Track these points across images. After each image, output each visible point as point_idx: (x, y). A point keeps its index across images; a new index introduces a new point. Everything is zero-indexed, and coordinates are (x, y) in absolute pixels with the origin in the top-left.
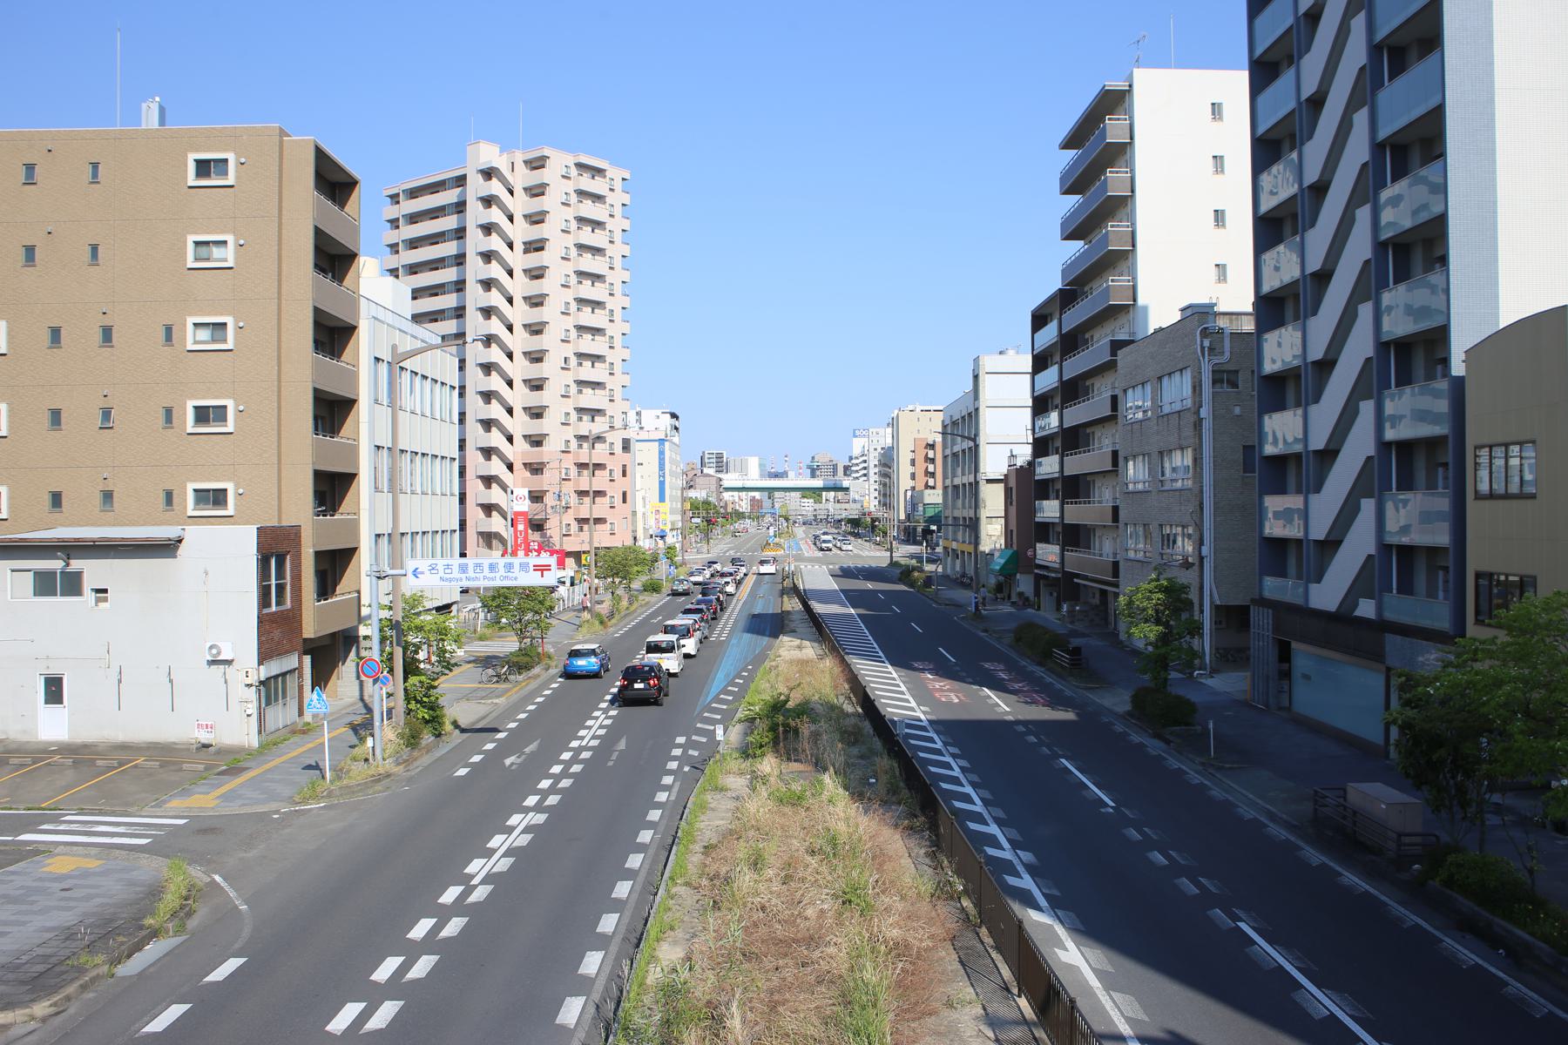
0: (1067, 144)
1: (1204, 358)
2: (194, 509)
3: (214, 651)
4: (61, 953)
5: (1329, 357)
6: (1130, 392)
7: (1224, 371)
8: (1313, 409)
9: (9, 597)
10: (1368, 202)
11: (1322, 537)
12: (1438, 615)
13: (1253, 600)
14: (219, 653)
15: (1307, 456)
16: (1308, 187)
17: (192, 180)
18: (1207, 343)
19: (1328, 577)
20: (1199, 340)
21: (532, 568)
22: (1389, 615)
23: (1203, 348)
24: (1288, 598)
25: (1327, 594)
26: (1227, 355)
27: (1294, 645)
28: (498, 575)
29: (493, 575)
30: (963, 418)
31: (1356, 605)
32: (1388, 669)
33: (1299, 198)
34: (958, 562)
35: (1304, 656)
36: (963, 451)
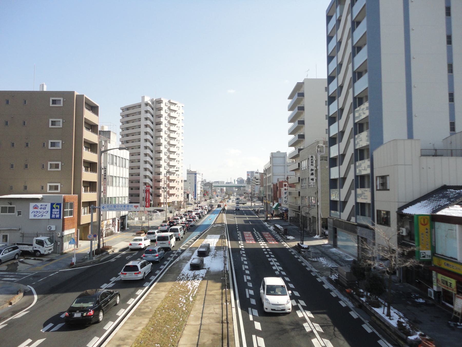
3: (50, 228)
7: (323, 157)
8: (341, 166)
10: (353, 138)
15: (340, 179)
18: (319, 149)
21: (134, 206)
22: (358, 222)
23: (318, 151)
27: (338, 229)
32: (358, 236)
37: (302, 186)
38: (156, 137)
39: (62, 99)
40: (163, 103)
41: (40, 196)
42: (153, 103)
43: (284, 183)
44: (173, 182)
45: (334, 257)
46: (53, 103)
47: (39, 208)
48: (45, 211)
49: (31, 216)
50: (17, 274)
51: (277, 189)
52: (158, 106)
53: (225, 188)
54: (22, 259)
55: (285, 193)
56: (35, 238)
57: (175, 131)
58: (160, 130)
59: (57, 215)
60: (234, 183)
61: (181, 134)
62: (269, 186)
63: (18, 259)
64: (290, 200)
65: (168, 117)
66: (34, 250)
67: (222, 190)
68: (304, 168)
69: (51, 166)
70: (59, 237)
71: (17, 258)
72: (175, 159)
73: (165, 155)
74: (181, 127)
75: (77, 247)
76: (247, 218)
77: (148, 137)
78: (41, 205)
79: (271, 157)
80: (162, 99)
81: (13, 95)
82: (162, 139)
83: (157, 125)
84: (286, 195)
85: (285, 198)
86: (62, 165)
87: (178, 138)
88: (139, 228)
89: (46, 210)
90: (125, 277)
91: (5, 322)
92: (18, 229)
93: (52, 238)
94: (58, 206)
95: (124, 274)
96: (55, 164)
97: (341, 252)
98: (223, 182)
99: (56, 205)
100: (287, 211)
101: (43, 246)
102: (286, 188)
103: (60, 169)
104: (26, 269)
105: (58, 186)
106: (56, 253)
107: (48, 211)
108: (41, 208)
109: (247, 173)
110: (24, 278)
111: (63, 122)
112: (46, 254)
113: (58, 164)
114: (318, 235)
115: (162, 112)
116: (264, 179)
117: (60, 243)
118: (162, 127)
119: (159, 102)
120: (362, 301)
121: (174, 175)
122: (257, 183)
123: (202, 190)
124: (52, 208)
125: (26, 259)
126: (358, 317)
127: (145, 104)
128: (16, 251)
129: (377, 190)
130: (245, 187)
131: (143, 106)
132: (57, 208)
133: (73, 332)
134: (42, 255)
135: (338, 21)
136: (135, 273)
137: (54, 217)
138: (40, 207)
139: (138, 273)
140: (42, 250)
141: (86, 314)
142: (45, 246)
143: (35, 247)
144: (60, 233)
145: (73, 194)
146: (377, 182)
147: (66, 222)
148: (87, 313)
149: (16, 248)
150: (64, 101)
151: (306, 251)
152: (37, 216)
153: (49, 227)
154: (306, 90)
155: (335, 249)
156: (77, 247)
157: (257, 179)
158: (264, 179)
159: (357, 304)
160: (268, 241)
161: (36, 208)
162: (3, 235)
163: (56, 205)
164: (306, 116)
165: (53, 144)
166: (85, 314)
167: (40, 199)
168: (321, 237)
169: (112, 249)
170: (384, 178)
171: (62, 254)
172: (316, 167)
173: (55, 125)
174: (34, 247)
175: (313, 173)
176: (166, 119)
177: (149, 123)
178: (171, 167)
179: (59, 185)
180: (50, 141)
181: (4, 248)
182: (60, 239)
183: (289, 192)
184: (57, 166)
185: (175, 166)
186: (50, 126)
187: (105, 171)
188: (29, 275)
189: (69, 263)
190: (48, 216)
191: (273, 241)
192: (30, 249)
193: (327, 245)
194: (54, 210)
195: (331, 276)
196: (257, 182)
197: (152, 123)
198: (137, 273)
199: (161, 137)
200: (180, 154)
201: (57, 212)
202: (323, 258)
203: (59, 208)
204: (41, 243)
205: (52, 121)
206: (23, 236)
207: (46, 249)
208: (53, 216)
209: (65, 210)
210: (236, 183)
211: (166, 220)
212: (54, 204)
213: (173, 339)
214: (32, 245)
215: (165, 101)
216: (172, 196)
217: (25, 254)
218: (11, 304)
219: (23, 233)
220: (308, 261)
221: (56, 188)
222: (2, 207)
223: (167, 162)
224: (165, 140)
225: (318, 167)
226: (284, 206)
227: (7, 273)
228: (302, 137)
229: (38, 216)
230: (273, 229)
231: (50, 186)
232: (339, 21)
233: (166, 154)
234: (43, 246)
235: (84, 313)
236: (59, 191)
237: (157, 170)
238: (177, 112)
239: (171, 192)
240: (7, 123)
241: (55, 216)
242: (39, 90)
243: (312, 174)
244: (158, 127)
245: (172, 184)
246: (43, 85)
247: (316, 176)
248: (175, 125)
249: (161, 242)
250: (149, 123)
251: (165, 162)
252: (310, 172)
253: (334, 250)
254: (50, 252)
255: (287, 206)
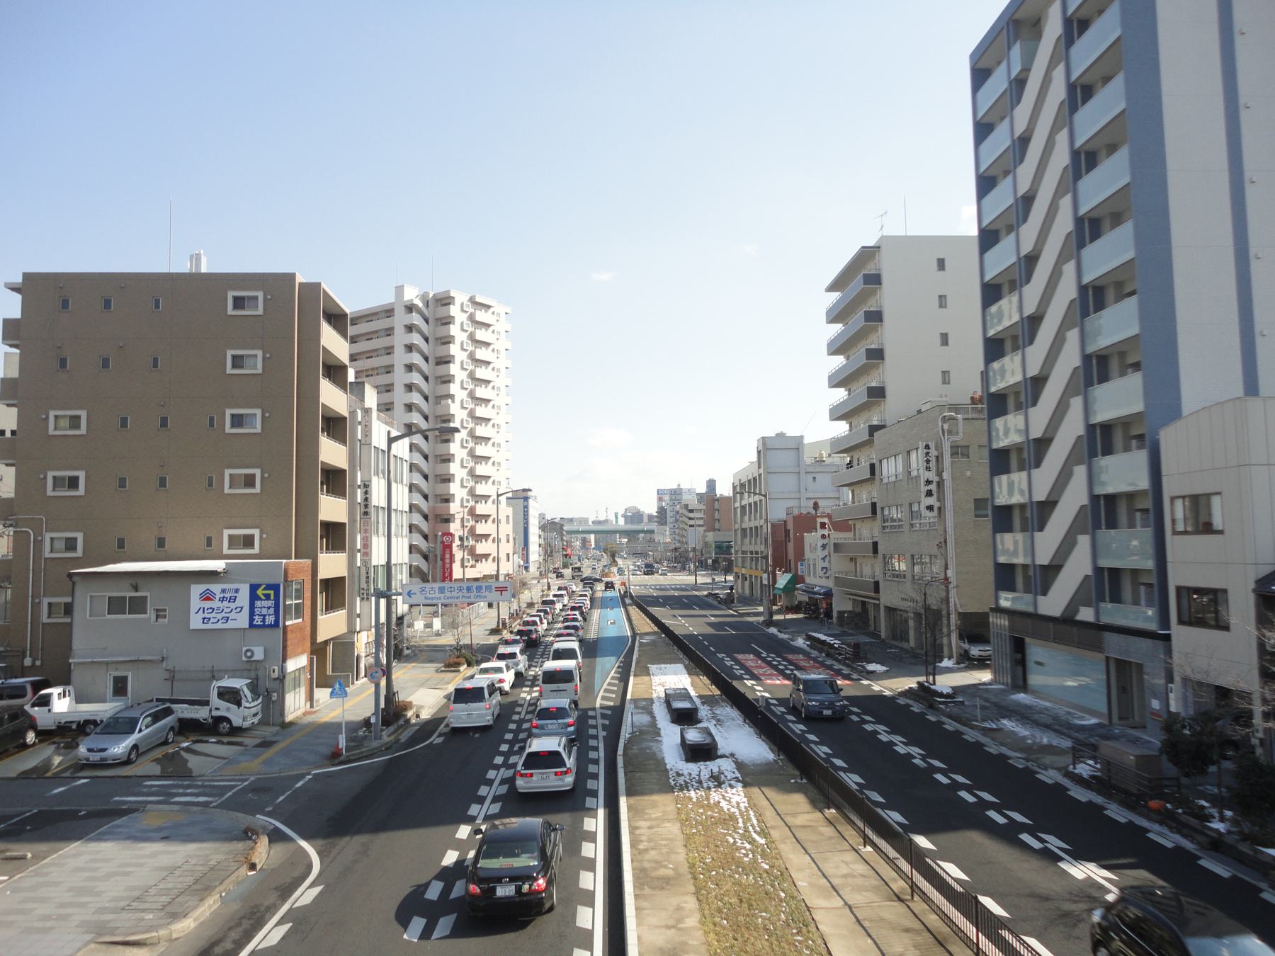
0: (832, 288)
1: (944, 435)
2: (229, 548)
3: (249, 654)
4: (179, 886)
5: (1051, 499)
6: (884, 462)
7: (958, 447)
9: (88, 616)
10: (1076, 326)
11: (1043, 499)
12: (1145, 617)
13: (992, 609)
14: (252, 655)
16: (1028, 316)
17: (230, 311)
18: (946, 427)
19: (1052, 592)
20: (940, 424)
21: (494, 589)
22: (1105, 619)
23: (943, 431)
24: (1021, 607)
25: (1053, 603)
26: (961, 434)
27: (1027, 640)
28: (472, 595)
29: (468, 595)
30: (749, 481)
31: (1077, 611)
32: (1107, 658)
33: (1027, 342)
34: (747, 583)
35: (1037, 651)
36: (750, 504)
37: (912, 525)
38: (437, 397)
39: (260, 295)
40: (454, 305)
41: (218, 565)
42: (427, 304)
43: (819, 520)
44: (484, 521)
45: (1036, 717)
46: (236, 307)
47: (218, 597)
48: (233, 605)
49: (196, 622)
50: (200, 783)
51: (786, 536)
52: (441, 312)
53: (592, 536)
54: (187, 744)
55: (824, 547)
56: (216, 684)
57: (489, 382)
58: (448, 380)
59: (267, 617)
60: (614, 522)
61: (503, 389)
62: (756, 528)
63: (173, 742)
64: (839, 565)
65: (469, 342)
66: (212, 717)
67: (584, 541)
68: (893, 479)
69: (57, 482)
70: (275, 679)
71: (170, 740)
72: (489, 458)
73: (462, 447)
74: (503, 370)
75: (312, 706)
76: (712, 616)
77: (416, 398)
78: (223, 591)
79: (761, 448)
80: (452, 294)
81: (61, 285)
82: (453, 402)
83: (438, 363)
84: (826, 552)
85: (823, 559)
86: (262, 478)
87: (496, 401)
88: (445, 651)
89: (238, 603)
90: (528, 785)
91: (282, 918)
92: (159, 658)
93: (255, 682)
94: (272, 592)
95: (526, 775)
96: (245, 475)
97: (1047, 704)
98: (586, 520)
99: (264, 589)
100: (828, 594)
101: (239, 704)
102: (826, 532)
103: (257, 489)
104: (215, 771)
105: (252, 536)
106: (267, 724)
107: (242, 608)
108: (222, 600)
109: (658, 494)
110: (230, 796)
111: (264, 358)
112: (248, 726)
113: (254, 476)
114: (949, 659)
115: (454, 330)
116: (735, 509)
117: (278, 696)
118: (454, 369)
119: (445, 301)
120: (1217, 831)
121: (486, 502)
122: (692, 522)
123: (542, 542)
124: (254, 597)
125: (195, 742)
126: (1230, 874)
127: (406, 307)
128: (169, 720)
129: (1175, 533)
130: (652, 532)
131: (400, 313)
132: (268, 597)
133: (499, 937)
134: (236, 731)
135: (1014, 84)
136: (556, 774)
137: (259, 623)
138: (219, 595)
139: (566, 773)
140: (238, 716)
141: (528, 886)
142: (244, 703)
143: (217, 709)
144: (276, 668)
145: (295, 558)
146: (1177, 513)
147: (290, 636)
148: (531, 885)
149: (168, 712)
150: (265, 300)
151: (950, 702)
152: (212, 620)
153: (247, 651)
154: (887, 266)
155: (1022, 694)
156: (312, 706)
157: (691, 511)
158: (735, 509)
159: (1201, 838)
160: (763, 678)
161: (208, 599)
162: (114, 677)
163: (264, 589)
164: (890, 336)
165: (238, 421)
166: (526, 888)
167: (220, 573)
168: (958, 663)
169: (414, 710)
170: (1198, 504)
171: (286, 726)
172: (939, 473)
173: (242, 367)
174: (213, 708)
175: (931, 491)
176: (465, 347)
177: (416, 359)
178: (479, 479)
179: (256, 532)
180: (229, 412)
181: (141, 715)
182: (276, 685)
183: (835, 544)
184: (249, 481)
185: (489, 477)
186: (229, 370)
187: (366, 493)
188: (235, 786)
189: (327, 751)
190: (242, 621)
191: (774, 678)
192: (201, 713)
193: (990, 684)
194: (258, 603)
195: (1075, 768)
196: (690, 519)
197: (426, 359)
198: (561, 773)
199: (452, 397)
200: (503, 444)
201: (269, 608)
202: (1010, 720)
203: (272, 597)
204: (231, 696)
205: (234, 357)
206: (173, 677)
207: (247, 712)
208: (258, 621)
209: (287, 603)
210: (621, 521)
211: (498, 625)
212: (260, 586)
213: (807, 947)
214: (206, 703)
215: (460, 298)
216: (484, 560)
217: (187, 727)
218: (253, 867)
219: (172, 669)
220: (972, 729)
221: (248, 541)
222: (109, 598)
223: (467, 467)
224: (462, 407)
225: (945, 475)
226: (817, 581)
227: (171, 782)
228: (878, 393)
229: (216, 620)
230: (808, 645)
231: (230, 536)
232: (1019, 84)
233: (465, 445)
234: (239, 704)
235: (524, 883)
236: (256, 550)
237: (440, 488)
238: (491, 328)
239: (481, 548)
240: (105, 364)
241: (264, 620)
242: (188, 271)
243: (929, 494)
244: (441, 370)
245: (481, 528)
246: (198, 257)
247: (941, 499)
248: (489, 363)
249: (554, 686)
250: (416, 359)
251: (462, 466)
252: (924, 489)
253: (1021, 697)
254: (256, 720)
255: (830, 584)
